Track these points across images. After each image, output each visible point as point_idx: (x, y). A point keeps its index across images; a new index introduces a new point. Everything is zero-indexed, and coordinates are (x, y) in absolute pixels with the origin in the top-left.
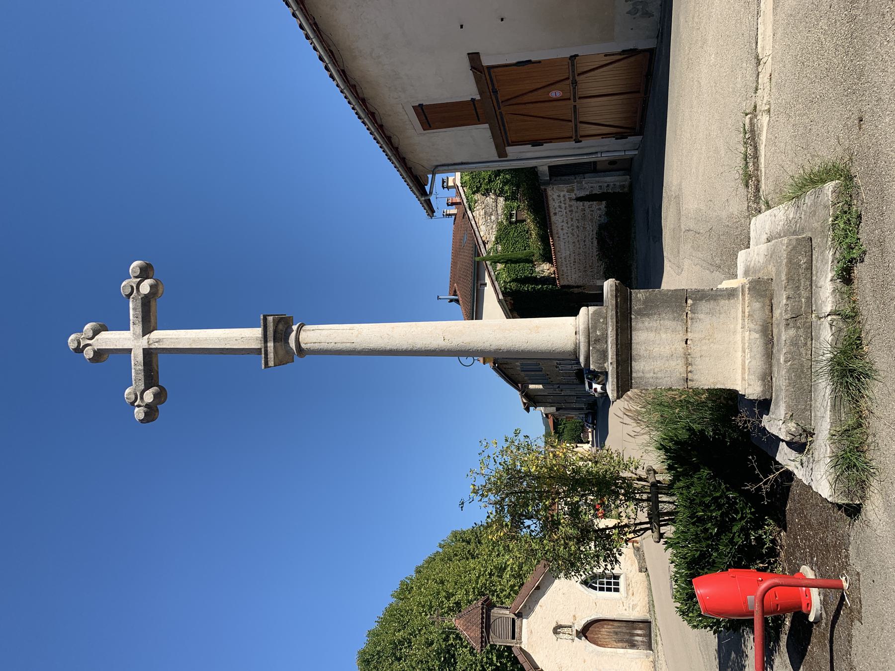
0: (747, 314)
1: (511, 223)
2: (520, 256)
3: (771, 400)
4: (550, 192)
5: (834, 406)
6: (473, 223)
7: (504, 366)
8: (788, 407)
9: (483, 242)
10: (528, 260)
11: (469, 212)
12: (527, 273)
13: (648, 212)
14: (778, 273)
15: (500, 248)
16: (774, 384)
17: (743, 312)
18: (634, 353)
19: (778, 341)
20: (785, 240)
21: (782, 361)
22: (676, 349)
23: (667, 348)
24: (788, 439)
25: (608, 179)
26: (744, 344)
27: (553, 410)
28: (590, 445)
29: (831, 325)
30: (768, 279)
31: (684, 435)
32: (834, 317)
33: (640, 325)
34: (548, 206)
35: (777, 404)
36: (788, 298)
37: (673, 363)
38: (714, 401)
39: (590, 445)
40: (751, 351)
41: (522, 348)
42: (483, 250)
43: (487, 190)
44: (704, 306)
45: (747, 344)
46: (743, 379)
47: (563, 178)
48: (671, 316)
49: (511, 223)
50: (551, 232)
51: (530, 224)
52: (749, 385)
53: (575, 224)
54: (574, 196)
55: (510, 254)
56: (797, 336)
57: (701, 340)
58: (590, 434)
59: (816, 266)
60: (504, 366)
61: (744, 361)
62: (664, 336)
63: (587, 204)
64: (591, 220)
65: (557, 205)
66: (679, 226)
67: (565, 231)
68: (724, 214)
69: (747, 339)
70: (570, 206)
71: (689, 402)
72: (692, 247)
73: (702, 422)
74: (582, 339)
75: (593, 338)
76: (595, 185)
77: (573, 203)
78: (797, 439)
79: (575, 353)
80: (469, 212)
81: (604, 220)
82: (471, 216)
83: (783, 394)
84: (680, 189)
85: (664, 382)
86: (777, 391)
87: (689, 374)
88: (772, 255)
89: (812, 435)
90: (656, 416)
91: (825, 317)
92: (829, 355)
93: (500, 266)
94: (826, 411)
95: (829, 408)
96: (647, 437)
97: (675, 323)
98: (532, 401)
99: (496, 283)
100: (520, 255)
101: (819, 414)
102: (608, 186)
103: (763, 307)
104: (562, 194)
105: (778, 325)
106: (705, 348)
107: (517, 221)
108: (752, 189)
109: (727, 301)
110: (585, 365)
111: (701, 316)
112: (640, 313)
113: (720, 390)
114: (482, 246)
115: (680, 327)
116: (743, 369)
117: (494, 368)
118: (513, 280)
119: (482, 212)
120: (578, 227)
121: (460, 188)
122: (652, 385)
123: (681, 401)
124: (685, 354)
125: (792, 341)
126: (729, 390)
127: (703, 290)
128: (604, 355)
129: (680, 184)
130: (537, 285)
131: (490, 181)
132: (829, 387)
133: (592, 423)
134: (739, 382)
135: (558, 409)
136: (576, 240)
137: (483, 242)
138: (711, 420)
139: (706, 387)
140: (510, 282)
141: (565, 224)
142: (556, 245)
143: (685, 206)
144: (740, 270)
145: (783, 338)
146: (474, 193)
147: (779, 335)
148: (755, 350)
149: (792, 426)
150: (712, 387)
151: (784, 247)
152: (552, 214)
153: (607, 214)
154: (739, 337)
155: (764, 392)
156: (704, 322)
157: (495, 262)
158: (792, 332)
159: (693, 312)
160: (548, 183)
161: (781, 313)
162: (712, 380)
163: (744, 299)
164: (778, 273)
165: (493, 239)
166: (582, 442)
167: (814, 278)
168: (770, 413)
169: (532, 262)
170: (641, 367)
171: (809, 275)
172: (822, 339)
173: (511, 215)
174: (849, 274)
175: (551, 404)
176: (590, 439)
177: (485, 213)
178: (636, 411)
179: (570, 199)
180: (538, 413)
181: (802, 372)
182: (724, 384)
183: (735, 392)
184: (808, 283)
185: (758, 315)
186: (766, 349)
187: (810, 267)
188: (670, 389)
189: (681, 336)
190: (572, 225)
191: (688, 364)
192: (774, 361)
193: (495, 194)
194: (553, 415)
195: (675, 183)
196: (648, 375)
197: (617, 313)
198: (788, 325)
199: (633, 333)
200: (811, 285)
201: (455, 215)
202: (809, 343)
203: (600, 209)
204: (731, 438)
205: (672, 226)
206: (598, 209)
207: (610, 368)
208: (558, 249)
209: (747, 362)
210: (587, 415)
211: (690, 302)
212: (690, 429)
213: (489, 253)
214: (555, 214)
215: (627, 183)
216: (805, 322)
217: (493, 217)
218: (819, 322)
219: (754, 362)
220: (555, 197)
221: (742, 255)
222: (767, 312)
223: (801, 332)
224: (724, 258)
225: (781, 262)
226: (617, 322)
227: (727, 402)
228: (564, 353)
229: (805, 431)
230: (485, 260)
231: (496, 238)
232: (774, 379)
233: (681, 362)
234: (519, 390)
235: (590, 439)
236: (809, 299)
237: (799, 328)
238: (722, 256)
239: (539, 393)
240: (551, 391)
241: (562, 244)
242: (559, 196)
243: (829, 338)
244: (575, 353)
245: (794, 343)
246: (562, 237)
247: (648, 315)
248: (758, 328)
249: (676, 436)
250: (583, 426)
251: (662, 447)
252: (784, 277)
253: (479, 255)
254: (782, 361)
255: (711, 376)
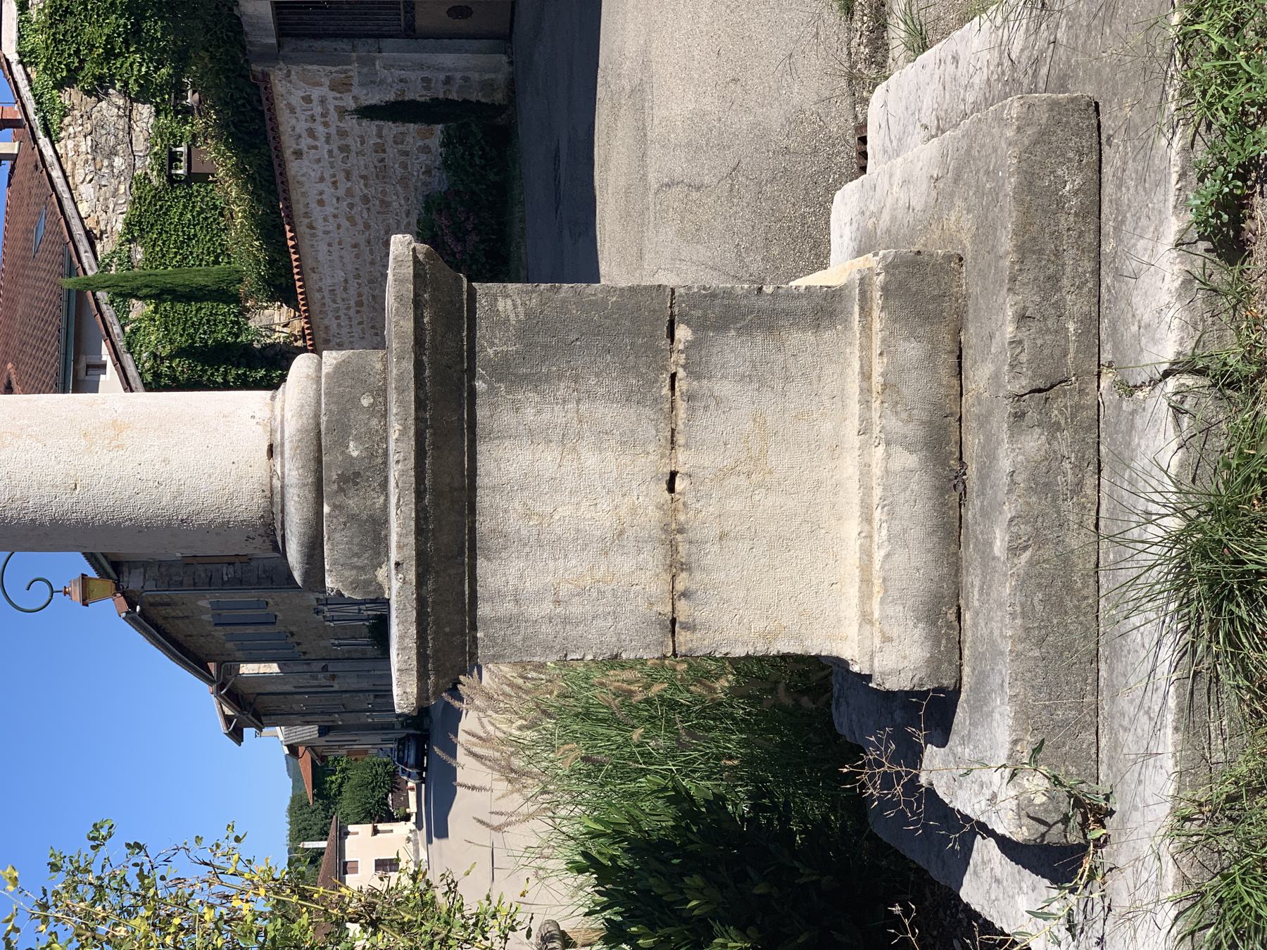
0: (877, 380)
1: (172, 180)
2: (200, 280)
3: (957, 691)
4: (279, 86)
5: (1188, 709)
6: (56, 173)
7: (164, 611)
8: (1024, 716)
9: (89, 234)
10: (223, 294)
11: (43, 141)
12: (222, 333)
13: (556, 158)
14: (986, 235)
15: (139, 254)
16: (968, 637)
17: (866, 376)
18: (484, 524)
19: (983, 477)
20: (1013, 107)
21: (999, 546)
22: (633, 511)
23: (604, 505)
24: (1021, 833)
25: (448, 60)
26: (866, 489)
27: (309, 732)
28: (411, 825)
29: (1177, 411)
30: (948, 258)
31: (659, 818)
32: (1188, 380)
33: (506, 418)
34: (275, 128)
35: (981, 707)
36: (1022, 318)
37: (624, 564)
38: (753, 700)
39: (411, 825)
40: (892, 514)
41: (54, 510)
42: (87, 258)
43: (100, 78)
44: (734, 351)
45: (878, 492)
46: (866, 618)
47: (318, 44)
48: (618, 386)
49: (172, 180)
50: (288, 208)
51: (230, 191)
52: (887, 639)
53: (359, 188)
54: (352, 105)
55: (169, 274)
56: (1052, 459)
57: (723, 474)
58: (412, 796)
59: (1117, 202)
60: (164, 611)
61: (867, 554)
62: (591, 460)
63: (391, 129)
64: (403, 181)
65: (302, 127)
66: (644, 177)
67: (329, 210)
68: (775, 116)
69: (877, 471)
70: (342, 134)
71: (673, 705)
72: (681, 233)
73: (716, 775)
74: (293, 472)
75: (329, 464)
76: (411, 75)
77: (351, 123)
78: (1055, 836)
79: (269, 528)
80: (43, 141)
81: (440, 181)
82: (48, 152)
83: (1004, 670)
84: (646, 65)
85: (593, 635)
86: (978, 657)
87: (682, 605)
88: (956, 176)
89: (1101, 815)
90: (569, 756)
91: (1154, 383)
92: (1175, 523)
93: (139, 309)
94: (1157, 729)
95: (1170, 718)
96: (541, 826)
97: (631, 411)
98: (247, 709)
99: (127, 359)
100: (200, 276)
101: (1128, 739)
102: (448, 81)
103: (931, 356)
104: (316, 93)
105: (983, 421)
106: (735, 505)
107: (191, 177)
108: (862, 22)
109: (809, 336)
110: (306, 575)
111: (724, 388)
112: (505, 372)
113: (785, 657)
114: (83, 246)
115: (648, 426)
116: (866, 581)
117: (131, 618)
118: (180, 353)
119: (85, 145)
120: (366, 200)
121: (17, 70)
122: (548, 648)
123: (649, 701)
124: (665, 529)
125: (1033, 477)
126: (817, 658)
127: (728, 293)
128: (373, 532)
129: (645, 51)
130: (252, 367)
131: (110, 54)
132: (1169, 640)
133: (419, 765)
134: (852, 629)
135: (323, 731)
136: (361, 239)
137: (89, 234)
138: (748, 761)
139: (739, 652)
140: (171, 357)
141: (327, 188)
142: (305, 248)
143: (660, 113)
144: (842, 234)
145: (1005, 464)
146: (59, 86)
147: (990, 455)
148: (904, 510)
149: (1036, 785)
150: (760, 649)
151: (1010, 133)
152: (288, 153)
153: (446, 165)
154: (849, 468)
155: (934, 663)
156: (733, 412)
157: (124, 294)
158: (1034, 442)
159: (693, 374)
160: (272, 56)
161: (996, 377)
162: (759, 625)
163: (866, 329)
164: (985, 231)
165: (120, 227)
166: (391, 818)
167: (1107, 248)
168: (954, 739)
169: (235, 299)
170: (510, 582)
171: (1090, 238)
172: (1141, 462)
173: (174, 158)
174: (1236, 222)
175: (304, 718)
176: (413, 808)
177: (95, 147)
178: (508, 741)
179: (342, 112)
180: (270, 744)
181: (1069, 587)
182: (799, 638)
183: (839, 665)
184: (1088, 265)
185: (916, 387)
186: (941, 507)
187: (1093, 208)
188: (614, 661)
189: (651, 462)
190: (349, 192)
191: (676, 566)
192: (969, 553)
193: (125, 92)
194: (311, 747)
195: (631, 48)
196: (534, 611)
197: (419, 366)
198: (1019, 416)
199: (481, 448)
200: (1097, 272)
201: (13, 158)
202: (1090, 481)
203: (426, 149)
204: (804, 820)
205: (622, 182)
206: (421, 145)
207: (396, 585)
208: (309, 263)
209: (878, 555)
210: (402, 742)
211: (683, 333)
212: (680, 798)
213: (104, 267)
214: (298, 154)
215: (500, 78)
216: (1078, 407)
217: (118, 162)
218: (1127, 406)
219: (900, 558)
220: (296, 100)
221: (846, 205)
222: (945, 374)
223: (1063, 443)
224: (775, 251)
225: (996, 192)
226: (420, 404)
227: (805, 703)
228: (223, 528)
229: (1078, 803)
230: (93, 286)
231: (128, 225)
232: (967, 616)
233: (653, 558)
234: (210, 681)
235: (413, 808)
236: (1091, 324)
237: (1056, 427)
238: (767, 247)
239: (270, 689)
240: (304, 680)
241: (323, 248)
242: (307, 99)
243: (1172, 459)
244: (269, 528)
245: (1041, 481)
246: (320, 224)
247: (535, 381)
248: (913, 431)
249: (634, 821)
250: (393, 775)
251: (587, 863)
252: (1006, 242)
253: (71, 272)
254: (999, 546)
255: (751, 616)
